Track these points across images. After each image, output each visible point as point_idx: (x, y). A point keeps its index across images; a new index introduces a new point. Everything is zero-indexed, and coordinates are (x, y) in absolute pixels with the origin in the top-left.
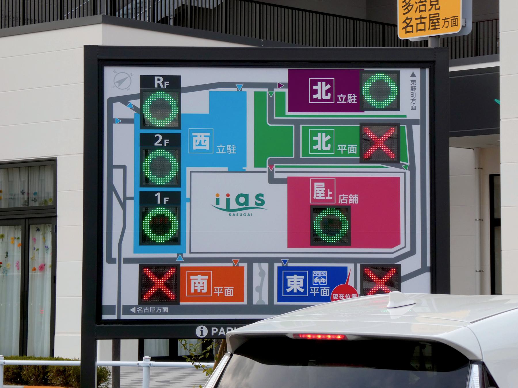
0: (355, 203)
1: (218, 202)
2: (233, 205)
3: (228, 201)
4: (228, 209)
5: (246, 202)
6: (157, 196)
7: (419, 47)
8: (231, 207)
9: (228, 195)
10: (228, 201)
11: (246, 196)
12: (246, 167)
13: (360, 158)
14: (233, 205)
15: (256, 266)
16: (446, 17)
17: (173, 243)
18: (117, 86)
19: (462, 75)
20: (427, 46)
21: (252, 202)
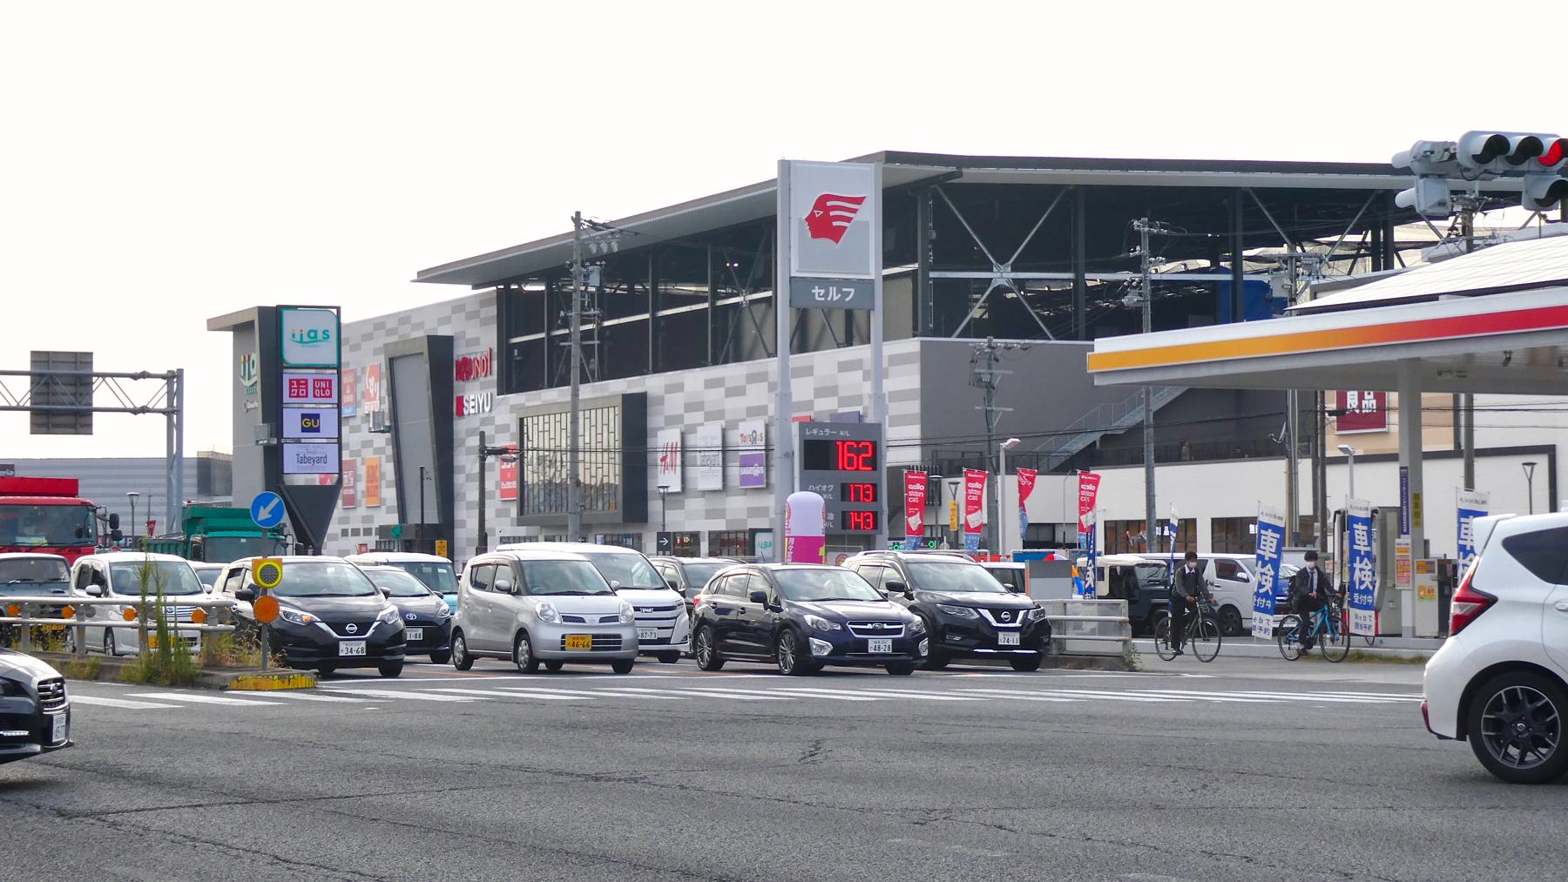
0: (1356, 531)
1: (293, 336)
2: (306, 338)
3: (302, 335)
4: (301, 341)
5: (316, 335)
6: (215, 325)
7: (1077, 549)
8: (304, 341)
9: (301, 331)
10: (302, 335)
11: (316, 332)
12: (745, 394)
13: (617, 252)
14: (306, 338)
15: (335, 371)
16: (1445, 555)
17: (1078, 494)
18: (756, 317)
19: (1032, 553)
20: (1326, 551)
21: (320, 336)
